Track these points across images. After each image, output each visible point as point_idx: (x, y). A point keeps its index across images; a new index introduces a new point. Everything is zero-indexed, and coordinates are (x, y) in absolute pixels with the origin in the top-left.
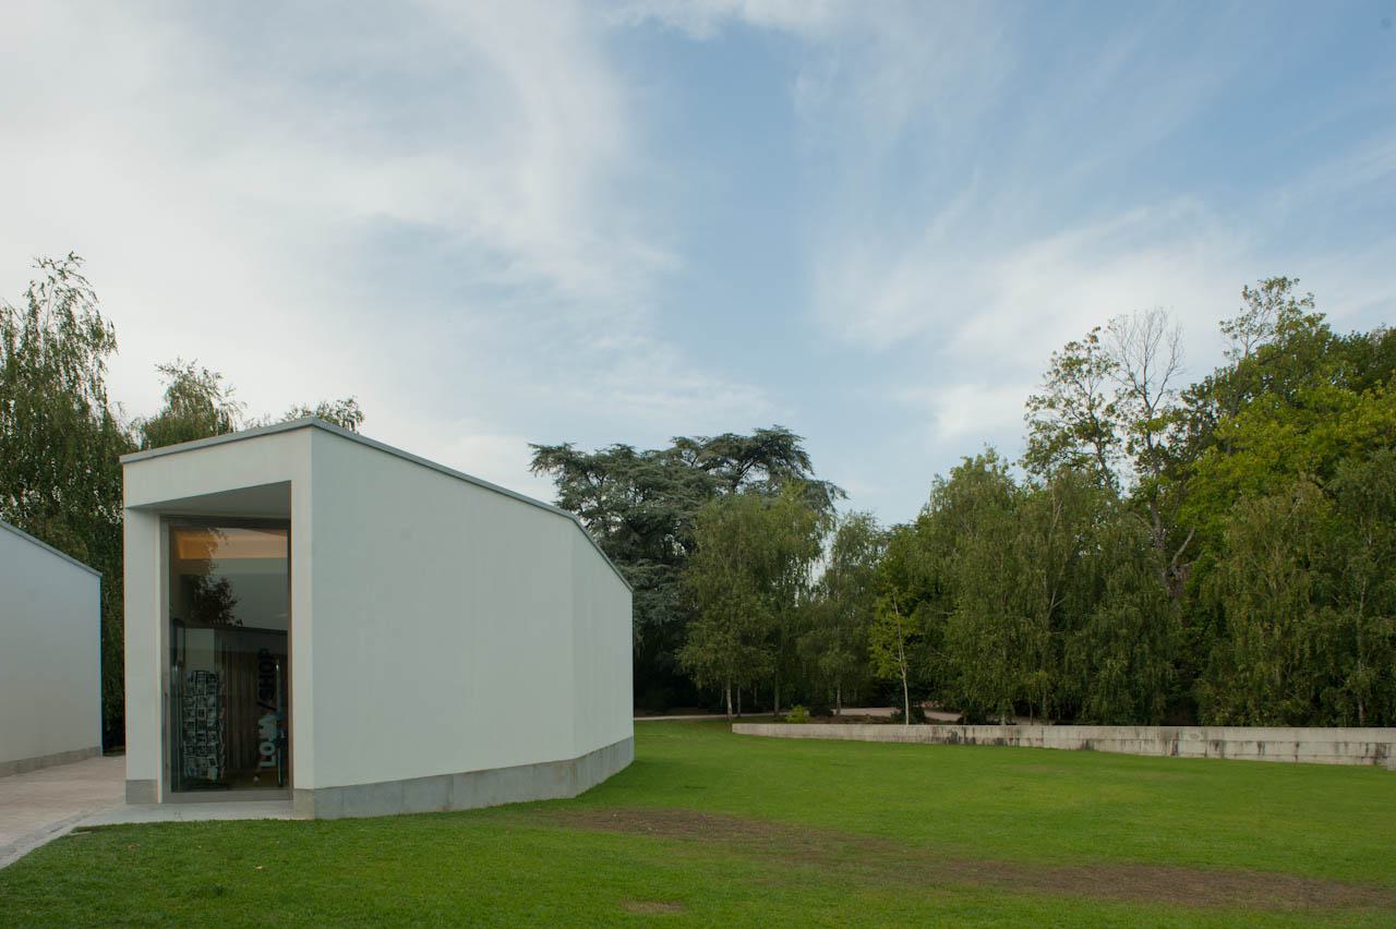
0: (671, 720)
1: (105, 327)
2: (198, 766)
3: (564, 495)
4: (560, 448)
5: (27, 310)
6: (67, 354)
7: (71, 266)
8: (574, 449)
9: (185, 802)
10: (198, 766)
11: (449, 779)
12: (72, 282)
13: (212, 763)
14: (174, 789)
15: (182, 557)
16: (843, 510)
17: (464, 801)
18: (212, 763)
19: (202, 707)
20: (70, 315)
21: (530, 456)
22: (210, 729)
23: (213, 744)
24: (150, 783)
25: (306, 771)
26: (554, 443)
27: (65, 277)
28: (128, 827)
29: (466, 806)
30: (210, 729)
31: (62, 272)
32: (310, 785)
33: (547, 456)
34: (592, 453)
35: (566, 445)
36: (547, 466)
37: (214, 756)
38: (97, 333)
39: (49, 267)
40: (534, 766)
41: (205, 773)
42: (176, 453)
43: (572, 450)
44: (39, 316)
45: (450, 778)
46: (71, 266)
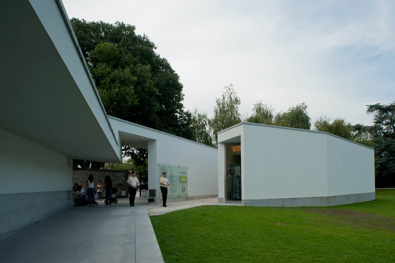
0: (393, 189)
1: (238, 99)
2: (236, 195)
3: (376, 119)
4: (376, 105)
5: (222, 98)
6: (232, 107)
7: (231, 87)
8: (381, 105)
9: (228, 203)
10: (236, 195)
11: (284, 200)
12: (231, 90)
13: (238, 195)
14: (227, 200)
15: (234, 151)
16: (274, 114)
17: (287, 205)
18: (238, 195)
19: (236, 183)
20: (231, 98)
21: (366, 108)
22: (238, 188)
23: (238, 191)
24: (222, 198)
25: (243, 197)
26: (374, 103)
27: (230, 90)
28: (217, 206)
29: (289, 206)
30: (238, 188)
31: (229, 89)
32: (244, 199)
33: (372, 108)
34: (389, 105)
35: (378, 104)
36: (372, 111)
37: (238, 194)
38: (237, 100)
39: (227, 88)
40: (313, 198)
41: (237, 197)
42: (239, 125)
43: (380, 105)
44: (225, 99)
45: (284, 199)
46: (231, 87)
